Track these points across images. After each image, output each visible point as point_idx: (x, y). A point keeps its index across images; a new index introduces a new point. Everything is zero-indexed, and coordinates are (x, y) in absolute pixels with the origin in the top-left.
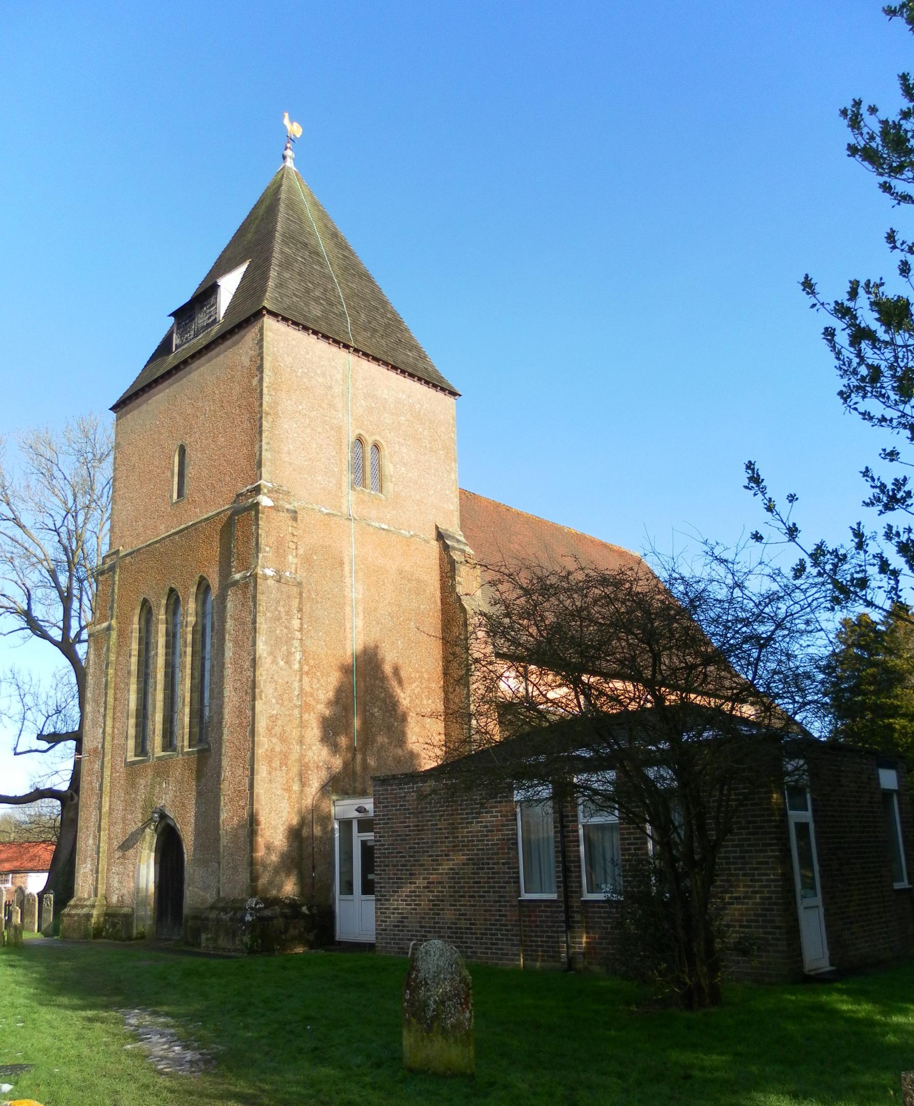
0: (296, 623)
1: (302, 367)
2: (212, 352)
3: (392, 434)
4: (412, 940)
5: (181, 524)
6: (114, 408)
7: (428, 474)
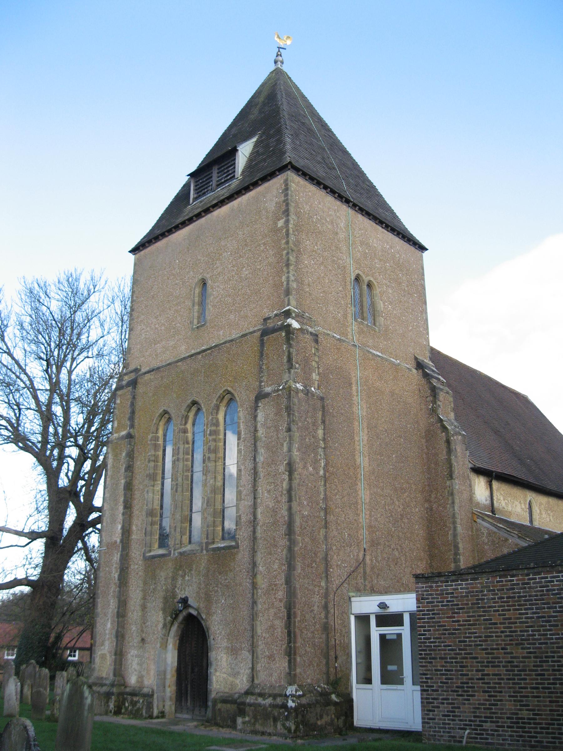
0: (320, 432)
1: (316, 215)
2: (244, 197)
3: (381, 277)
4: (466, 729)
5: (203, 346)
6: (134, 251)
7: (407, 312)
